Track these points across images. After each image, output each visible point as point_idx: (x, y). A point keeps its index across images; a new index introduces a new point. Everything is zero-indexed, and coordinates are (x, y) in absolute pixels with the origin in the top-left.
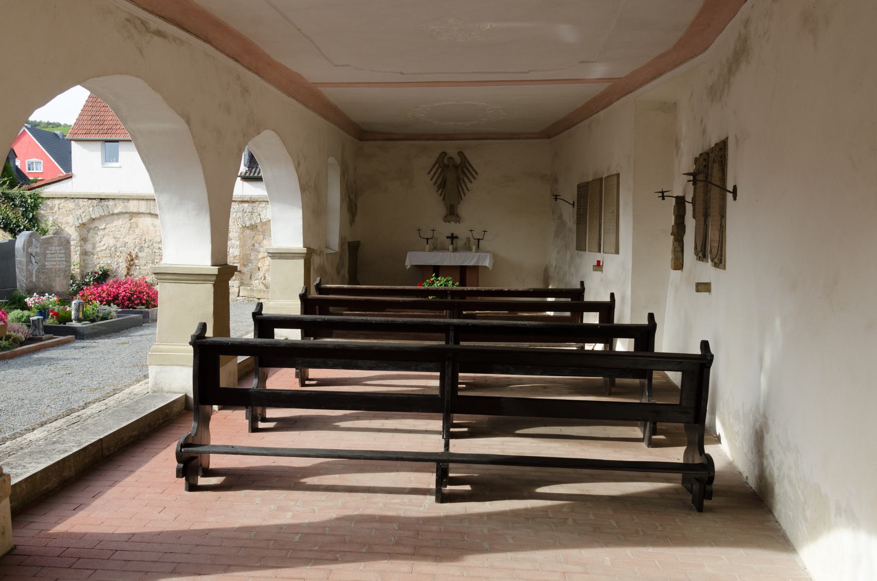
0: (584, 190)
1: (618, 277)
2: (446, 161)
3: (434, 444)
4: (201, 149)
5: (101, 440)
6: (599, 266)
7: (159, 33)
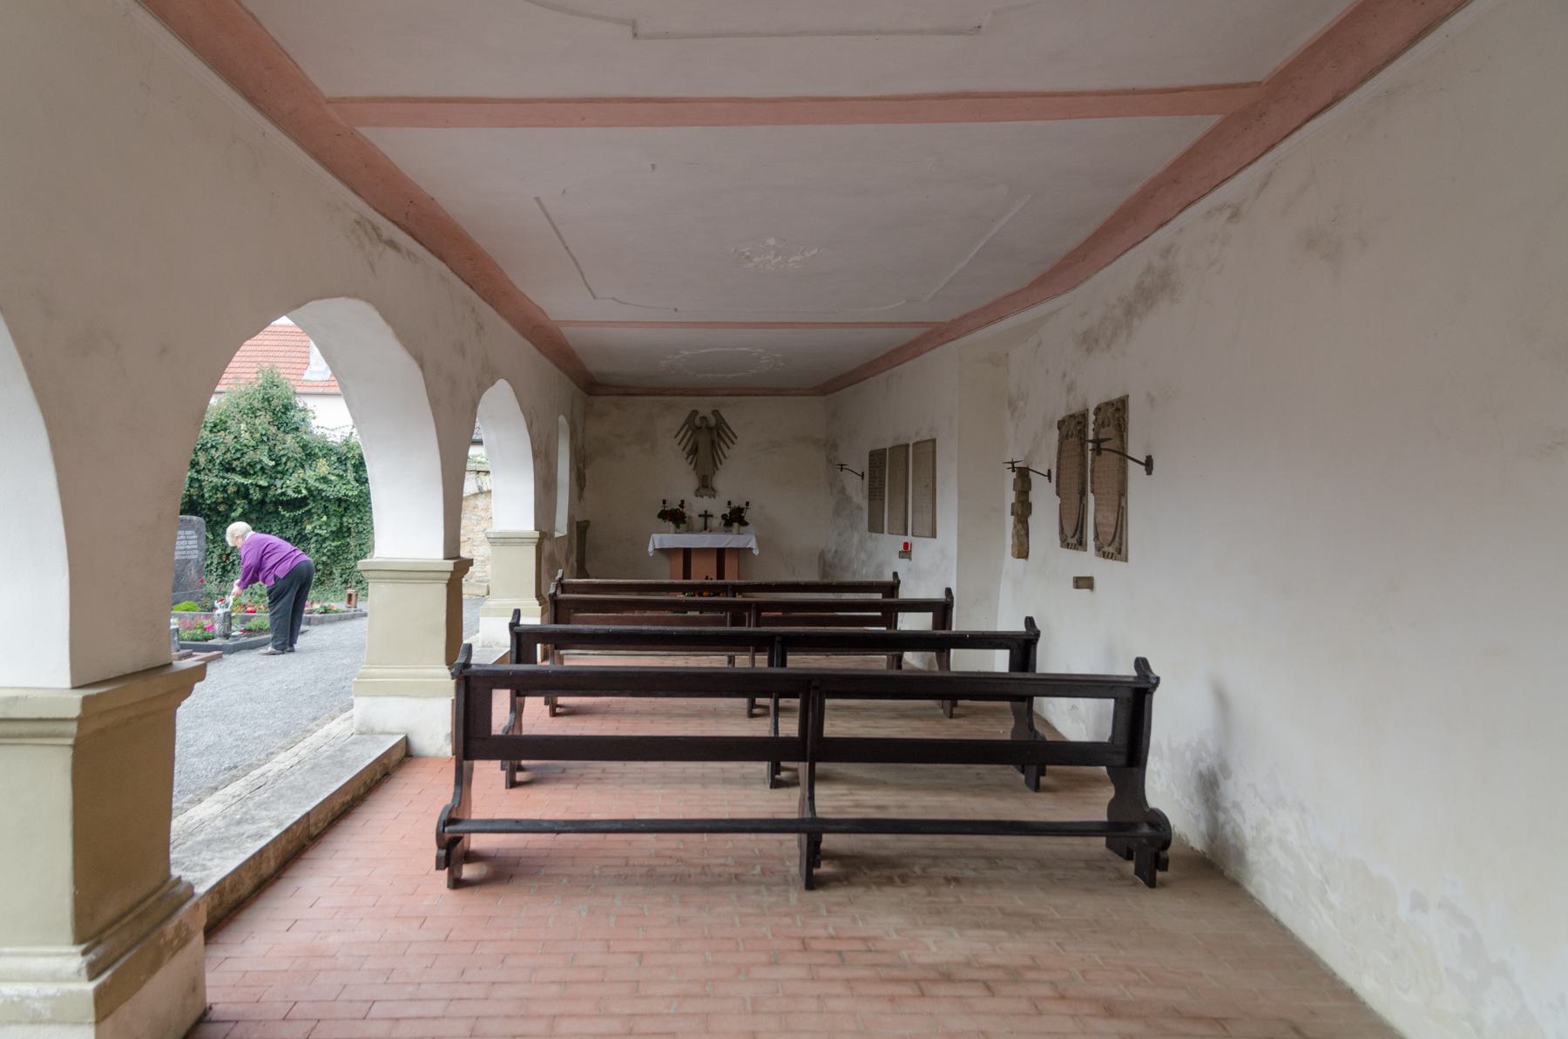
0: (877, 458)
1: (966, 568)
2: (697, 422)
3: (786, 804)
4: (434, 403)
5: (308, 815)
6: (906, 552)
7: (392, 244)
